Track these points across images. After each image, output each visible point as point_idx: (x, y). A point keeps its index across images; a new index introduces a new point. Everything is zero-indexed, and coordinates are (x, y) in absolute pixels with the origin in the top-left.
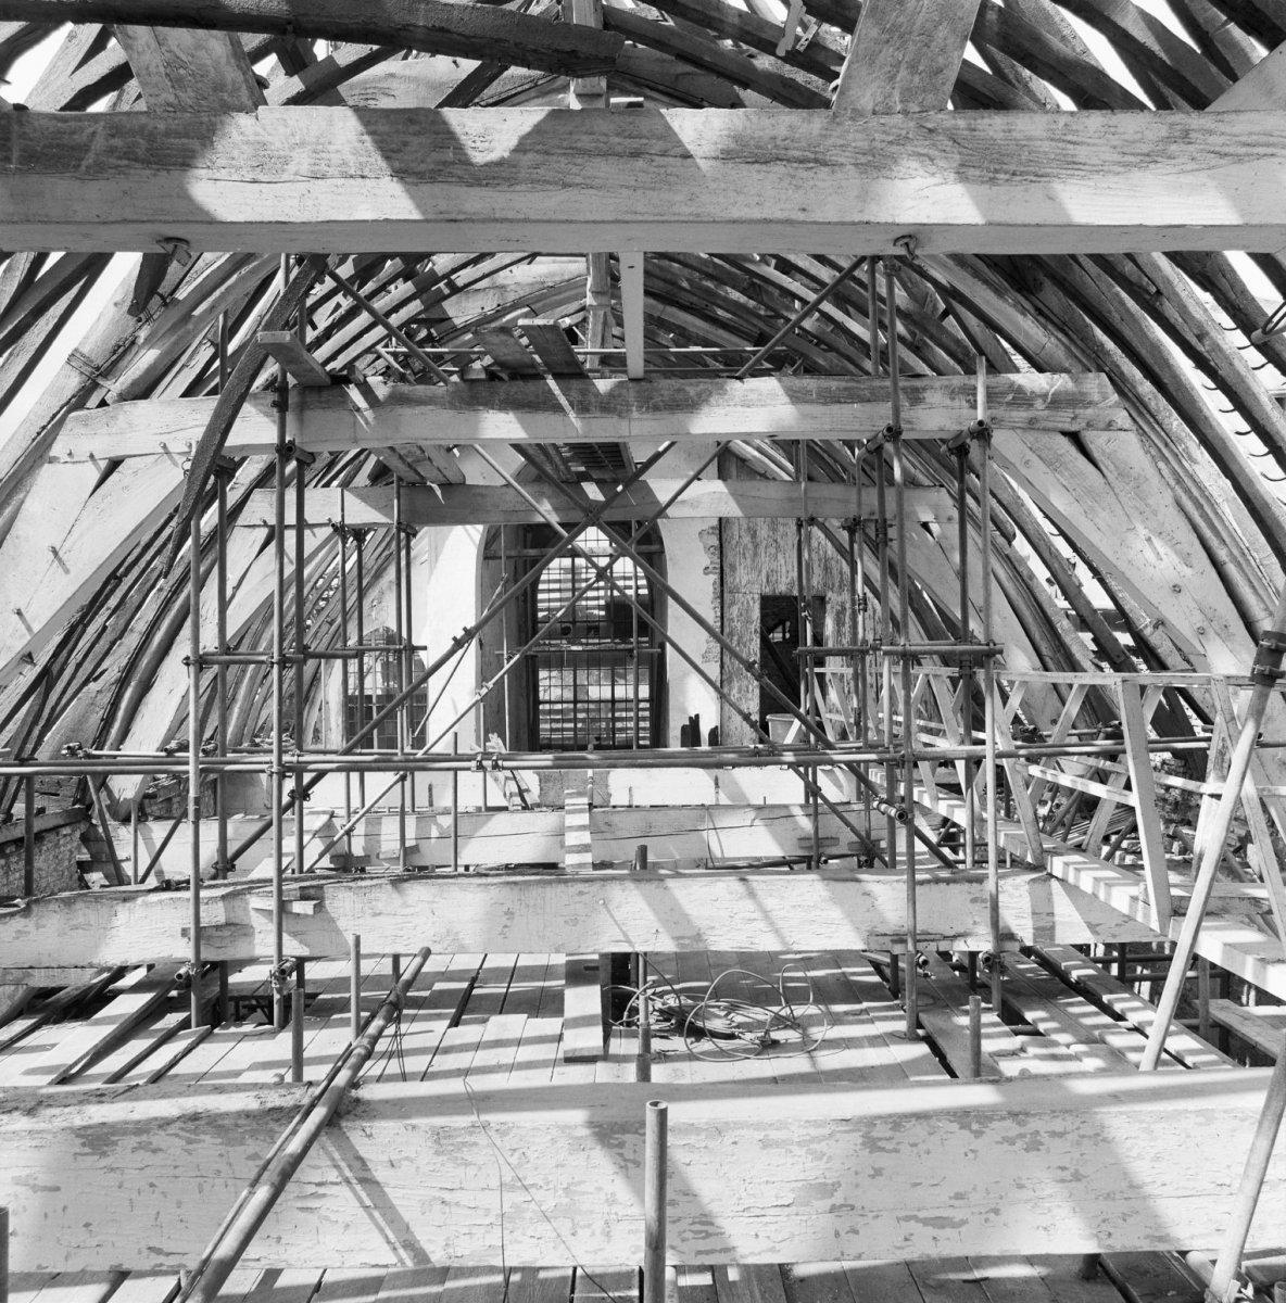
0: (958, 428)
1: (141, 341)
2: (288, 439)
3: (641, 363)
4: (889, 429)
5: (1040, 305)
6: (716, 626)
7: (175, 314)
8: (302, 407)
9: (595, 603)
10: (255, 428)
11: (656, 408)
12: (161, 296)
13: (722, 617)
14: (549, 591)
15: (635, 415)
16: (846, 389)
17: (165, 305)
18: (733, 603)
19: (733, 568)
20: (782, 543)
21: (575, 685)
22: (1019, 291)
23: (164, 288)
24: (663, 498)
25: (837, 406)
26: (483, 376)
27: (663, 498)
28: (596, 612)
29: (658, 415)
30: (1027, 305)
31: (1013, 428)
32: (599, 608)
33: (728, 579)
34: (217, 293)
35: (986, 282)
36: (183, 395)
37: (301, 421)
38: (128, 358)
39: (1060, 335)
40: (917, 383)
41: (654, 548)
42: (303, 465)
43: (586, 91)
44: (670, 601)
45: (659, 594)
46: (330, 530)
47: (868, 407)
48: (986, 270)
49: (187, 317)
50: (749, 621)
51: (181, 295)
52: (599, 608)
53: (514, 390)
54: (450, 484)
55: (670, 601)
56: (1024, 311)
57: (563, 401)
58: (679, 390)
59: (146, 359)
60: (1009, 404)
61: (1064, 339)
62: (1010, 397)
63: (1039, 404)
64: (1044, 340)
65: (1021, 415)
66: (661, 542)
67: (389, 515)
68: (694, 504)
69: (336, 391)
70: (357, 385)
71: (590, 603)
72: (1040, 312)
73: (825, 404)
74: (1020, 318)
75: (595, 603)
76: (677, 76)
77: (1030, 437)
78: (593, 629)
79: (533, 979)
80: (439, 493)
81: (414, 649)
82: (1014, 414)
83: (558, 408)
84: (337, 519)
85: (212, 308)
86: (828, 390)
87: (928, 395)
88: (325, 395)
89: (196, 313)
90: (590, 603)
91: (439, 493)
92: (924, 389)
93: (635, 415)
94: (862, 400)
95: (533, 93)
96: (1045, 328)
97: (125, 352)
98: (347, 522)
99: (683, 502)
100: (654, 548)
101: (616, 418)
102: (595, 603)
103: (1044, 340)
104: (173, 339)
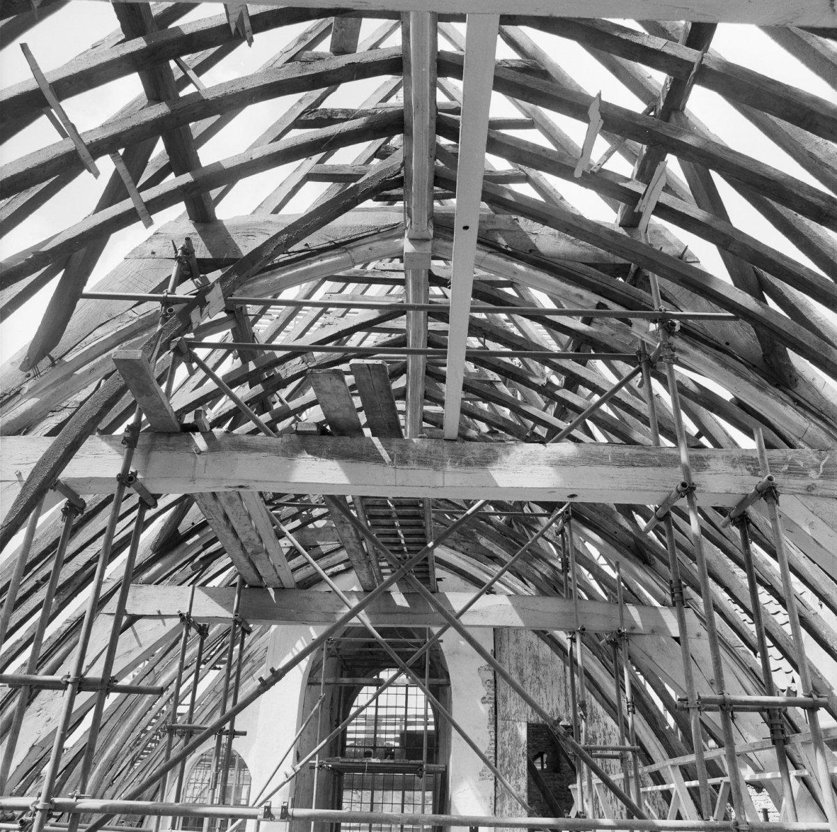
0: (743, 491)
1: (25, 391)
2: (132, 470)
3: (456, 427)
4: (684, 485)
5: (797, 397)
6: (490, 755)
7: (59, 373)
8: (150, 448)
9: (390, 738)
10: (99, 462)
11: (468, 464)
12: (52, 359)
13: (496, 741)
14: (356, 732)
15: (449, 468)
16: (638, 455)
17: (53, 365)
18: (505, 729)
19: (505, 699)
20: (543, 680)
21: (372, 803)
22: (777, 386)
23: (55, 353)
24: (458, 607)
25: (631, 469)
26: (315, 429)
27: (458, 607)
28: (392, 743)
29: (470, 469)
30: (786, 398)
31: (793, 494)
32: (395, 740)
33: (501, 708)
34: (99, 359)
35: (747, 379)
36: (47, 435)
37: (147, 460)
38: (9, 405)
39: (819, 422)
40: (701, 453)
41: (442, 681)
42: (144, 504)
43: (416, 237)
44: (454, 733)
45: (443, 719)
46: (177, 621)
47: (659, 470)
48: (746, 370)
49: (71, 374)
50: (517, 745)
51: (68, 359)
52: (395, 740)
53: (342, 443)
54: (284, 588)
55: (454, 733)
56: (784, 403)
57: (384, 454)
58: (489, 450)
59: (25, 405)
60: (785, 473)
61: (823, 425)
62: (786, 467)
63: (812, 473)
64: (806, 425)
65: (798, 483)
66: (448, 677)
67: (230, 610)
68: (483, 613)
69: (184, 436)
70: (203, 434)
71: (388, 736)
72: (799, 404)
73: (620, 466)
74: (781, 407)
75: (392, 736)
76: (487, 231)
77: (811, 502)
78: (388, 752)
79: (635, 314)
80: (272, 594)
81: (233, 734)
82: (791, 481)
83: (378, 459)
84: (185, 611)
85: (92, 370)
86: (622, 455)
87: (711, 463)
88: (173, 440)
89: (78, 372)
90: (388, 736)
91: (272, 594)
92: (708, 458)
93: (449, 468)
94: (654, 465)
95: (376, 238)
96: (805, 416)
97: (9, 399)
98: (192, 615)
99: (475, 611)
100: (442, 681)
101: (431, 470)
102: (392, 736)
103: (806, 425)
104: (53, 391)
